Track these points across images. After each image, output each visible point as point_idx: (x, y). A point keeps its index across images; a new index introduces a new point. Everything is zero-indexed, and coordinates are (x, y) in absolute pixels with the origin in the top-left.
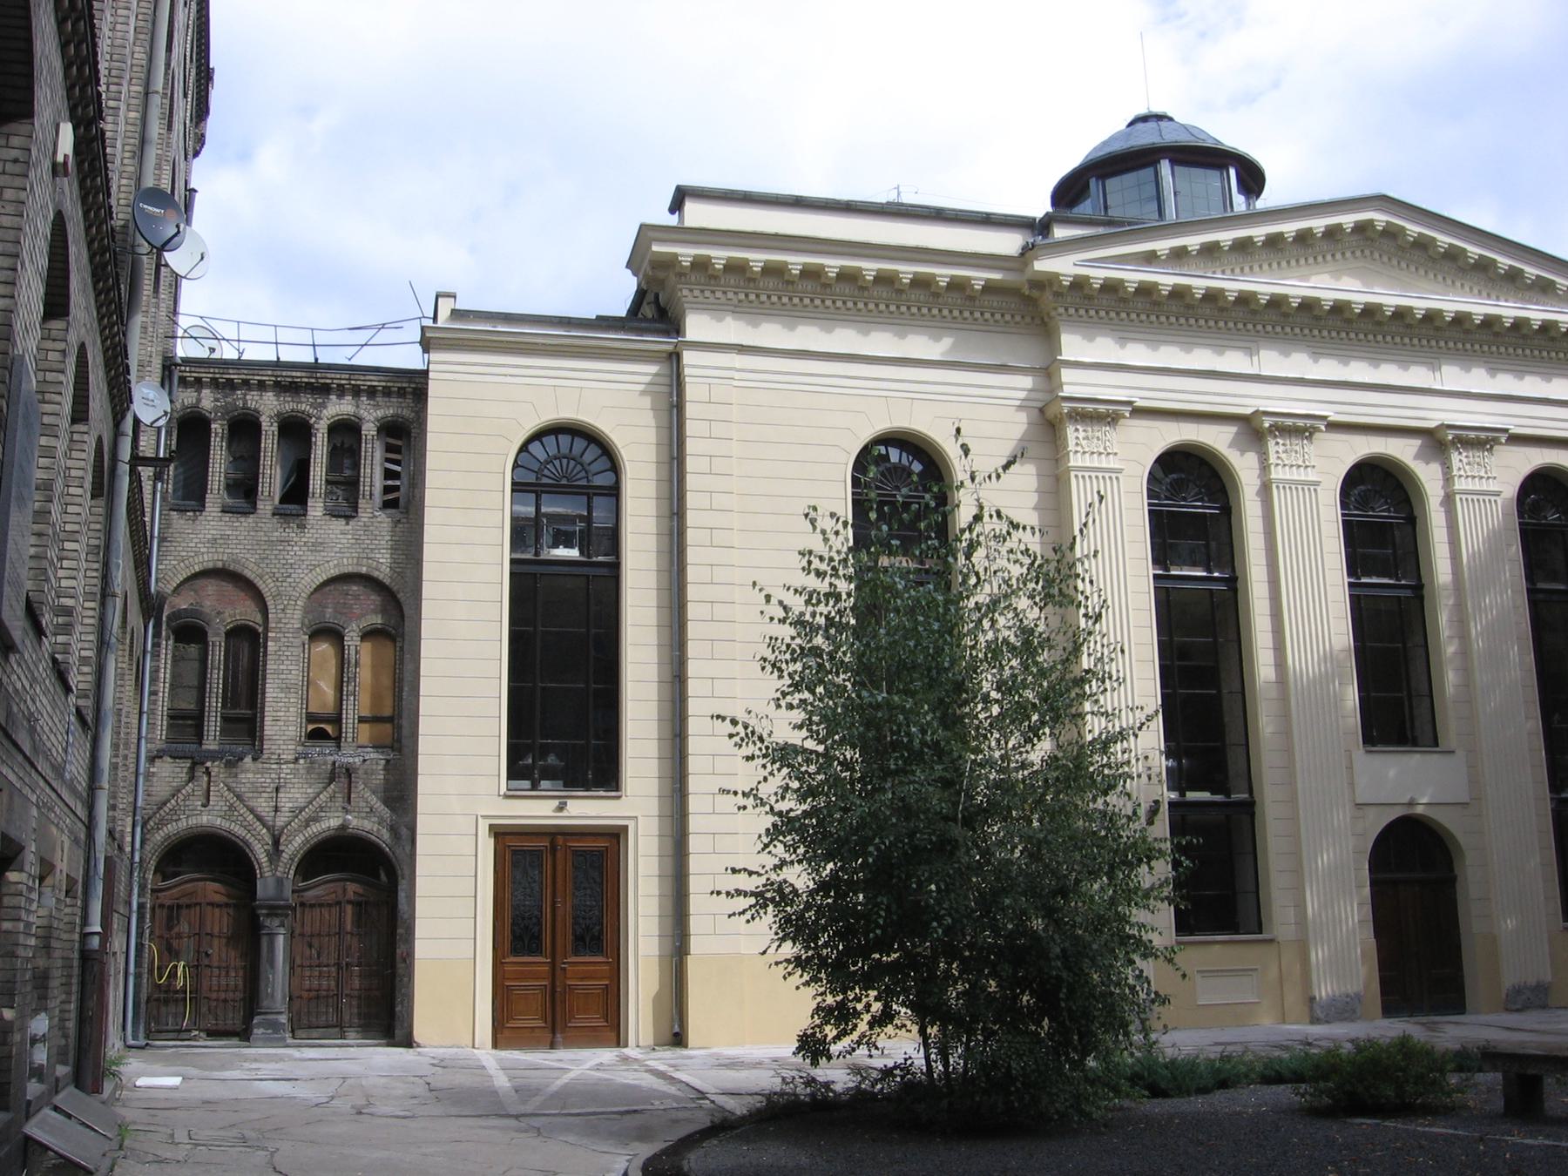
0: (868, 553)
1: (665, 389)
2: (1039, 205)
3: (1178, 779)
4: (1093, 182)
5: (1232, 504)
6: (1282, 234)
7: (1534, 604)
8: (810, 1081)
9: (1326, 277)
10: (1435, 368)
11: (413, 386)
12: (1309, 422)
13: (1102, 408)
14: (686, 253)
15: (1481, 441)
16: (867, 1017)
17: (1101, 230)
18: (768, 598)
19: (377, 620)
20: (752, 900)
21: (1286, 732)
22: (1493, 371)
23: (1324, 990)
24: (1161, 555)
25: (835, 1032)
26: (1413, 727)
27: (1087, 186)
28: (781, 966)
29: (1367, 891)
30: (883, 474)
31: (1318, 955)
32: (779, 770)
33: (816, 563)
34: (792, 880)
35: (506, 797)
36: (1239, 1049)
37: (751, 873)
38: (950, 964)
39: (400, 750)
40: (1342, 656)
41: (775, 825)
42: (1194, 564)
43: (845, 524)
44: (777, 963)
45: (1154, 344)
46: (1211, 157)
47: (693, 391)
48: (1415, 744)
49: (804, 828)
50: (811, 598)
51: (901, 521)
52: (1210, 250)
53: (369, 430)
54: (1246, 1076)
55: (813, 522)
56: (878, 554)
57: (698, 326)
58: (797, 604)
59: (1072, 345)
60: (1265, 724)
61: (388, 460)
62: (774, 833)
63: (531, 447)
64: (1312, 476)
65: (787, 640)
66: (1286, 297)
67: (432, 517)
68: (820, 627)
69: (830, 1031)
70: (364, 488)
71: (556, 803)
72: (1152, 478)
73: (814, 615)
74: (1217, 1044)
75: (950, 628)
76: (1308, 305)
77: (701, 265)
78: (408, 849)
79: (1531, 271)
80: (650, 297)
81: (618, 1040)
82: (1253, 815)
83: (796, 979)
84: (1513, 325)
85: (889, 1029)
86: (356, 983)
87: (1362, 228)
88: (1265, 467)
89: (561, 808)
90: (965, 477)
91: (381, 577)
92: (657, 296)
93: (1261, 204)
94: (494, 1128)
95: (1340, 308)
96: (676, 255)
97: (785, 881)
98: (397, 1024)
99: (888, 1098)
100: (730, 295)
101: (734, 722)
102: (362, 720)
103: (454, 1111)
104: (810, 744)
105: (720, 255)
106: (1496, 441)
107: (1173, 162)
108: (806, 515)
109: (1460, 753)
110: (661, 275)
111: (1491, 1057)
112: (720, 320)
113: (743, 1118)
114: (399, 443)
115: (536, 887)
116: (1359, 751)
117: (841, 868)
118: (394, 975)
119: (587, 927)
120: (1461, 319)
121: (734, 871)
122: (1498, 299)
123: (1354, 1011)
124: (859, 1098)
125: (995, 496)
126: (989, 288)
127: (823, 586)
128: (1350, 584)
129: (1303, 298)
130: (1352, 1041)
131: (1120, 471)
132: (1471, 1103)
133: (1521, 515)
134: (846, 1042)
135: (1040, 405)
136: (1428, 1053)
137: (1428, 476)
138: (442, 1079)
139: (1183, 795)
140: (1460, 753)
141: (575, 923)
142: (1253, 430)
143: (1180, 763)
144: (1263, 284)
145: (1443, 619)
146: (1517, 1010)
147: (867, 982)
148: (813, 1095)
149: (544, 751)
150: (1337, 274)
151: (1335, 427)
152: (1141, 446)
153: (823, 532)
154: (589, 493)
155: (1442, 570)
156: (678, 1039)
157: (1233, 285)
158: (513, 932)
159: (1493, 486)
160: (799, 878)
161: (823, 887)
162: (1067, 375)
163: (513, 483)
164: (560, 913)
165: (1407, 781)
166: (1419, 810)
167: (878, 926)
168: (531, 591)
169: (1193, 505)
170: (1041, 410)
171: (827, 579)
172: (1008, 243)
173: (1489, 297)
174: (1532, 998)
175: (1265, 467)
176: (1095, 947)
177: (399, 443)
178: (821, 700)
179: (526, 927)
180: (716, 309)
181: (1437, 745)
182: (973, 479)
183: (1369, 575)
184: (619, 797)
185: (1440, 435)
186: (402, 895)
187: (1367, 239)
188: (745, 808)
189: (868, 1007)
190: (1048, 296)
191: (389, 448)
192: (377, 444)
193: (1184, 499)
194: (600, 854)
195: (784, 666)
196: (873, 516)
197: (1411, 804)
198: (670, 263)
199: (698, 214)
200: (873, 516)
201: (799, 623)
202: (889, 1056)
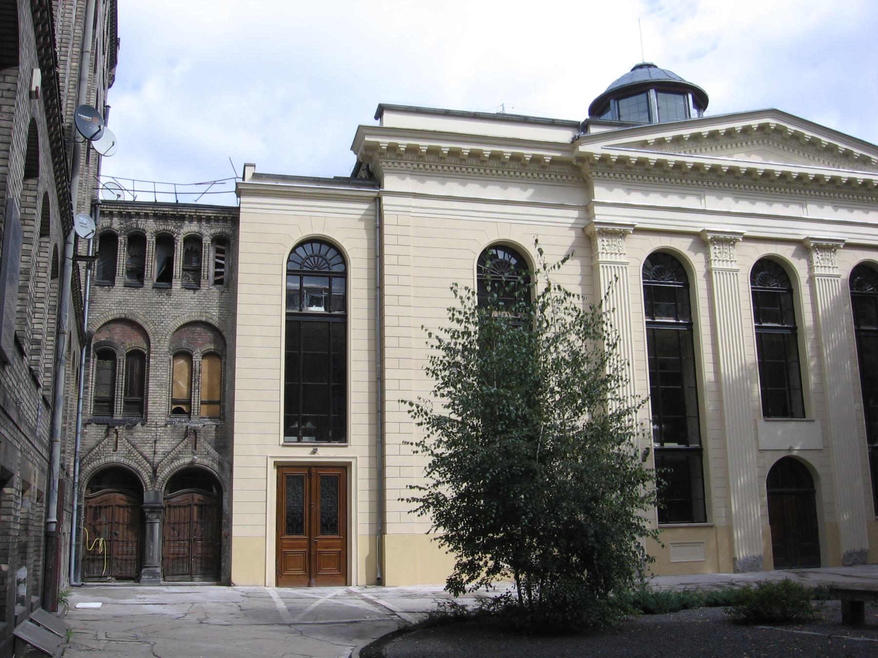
0: (486, 309)
1: (373, 218)
2: (582, 115)
3: (660, 436)
4: (612, 102)
5: (690, 282)
6: (718, 131)
7: (859, 338)
8: (454, 605)
9: (743, 155)
10: (803, 206)
11: (231, 216)
12: (733, 236)
13: (617, 228)
14: (384, 142)
15: (829, 247)
16: (485, 569)
17: (617, 129)
18: (430, 335)
19: (211, 347)
20: (421, 504)
21: (720, 409)
22: (836, 208)
23: (742, 554)
24: (650, 311)
25: (467, 578)
26: (791, 407)
27: (609, 104)
28: (437, 541)
29: (765, 498)
30: (494, 265)
31: (738, 534)
32: (436, 431)
33: (457, 315)
34: (443, 492)
35: (284, 446)
36: (694, 587)
37: (420, 489)
38: (532, 539)
39: (224, 420)
40: (752, 367)
41: (434, 462)
42: (669, 316)
43: (473, 293)
44: (435, 539)
45: (646, 192)
46: (678, 88)
47: (388, 219)
48: (792, 416)
49: (450, 463)
50: (454, 334)
51: (505, 292)
52: (678, 140)
53: (207, 240)
54: (698, 602)
55: (455, 292)
56: (491, 310)
57: (391, 182)
58: (447, 338)
59: (600, 193)
60: (708, 405)
61: (217, 257)
62: (434, 466)
63: (297, 250)
64: (734, 266)
65: (441, 358)
66: (720, 166)
67: (242, 289)
68: (459, 351)
69: (465, 577)
70: (204, 273)
71: (311, 449)
72: (645, 267)
73: (456, 344)
74: (681, 584)
75: (532, 352)
76: (733, 171)
77: (393, 148)
78: (228, 475)
79: (857, 152)
80: (364, 166)
81: (346, 582)
82: (701, 456)
83: (446, 548)
84: (847, 182)
85: (498, 576)
86: (200, 550)
87: (762, 128)
88: (708, 261)
89: (314, 452)
90: (540, 267)
91: (213, 323)
92: (368, 166)
93: (706, 114)
94: (276, 631)
95: (750, 172)
96: (378, 143)
97: (440, 493)
98: (223, 573)
99: (497, 614)
100: (409, 165)
101: (411, 404)
102: (203, 403)
103: (254, 622)
104: (454, 416)
105: (403, 143)
106: (838, 247)
107: (657, 91)
108: (452, 288)
109: (818, 421)
110: (370, 154)
111: (835, 591)
112: (403, 179)
113: (416, 625)
114: (224, 248)
115: (300, 496)
116: (761, 420)
117: (471, 486)
118: (220, 546)
119: (329, 519)
120: (818, 179)
121: (411, 487)
122: (839, 167)
123: (758, 566)
124: (481, 615)
125: (557, 278)
126: (554, 161)
127: (461, 328)
128: (756, 327)
129: (730, 167)
130: (757, 583)
131: (627, 263)
132: (824, 617)
133: (851, 288)
134: (473, 583)
135: (582, 226)
136: (799, 589)
137: (800, 266)
138: (247, 604)
139: (662, 445)
140: (818, 421)
141: (322, 517)
142: (702, 241)
143: (661, 427)
144: (707, 159)
145: (808, 346)
146: (850, 565)
147: (486, 549)
148: (455, 613)
149: (305, 420)
150: (748, 154)
151: (747, 239)
152: (639, 250)
153: (461, 298)
154: (330, 276)
155: (807, 319)
156: (380, 581)
157: (690, 160)
158: (287, 521)
159: (836, 272)
160: (448, 491)
161: (461, 496)
162: (597, 210)
163: (288, 271)
164: (313, 511)
165: (788, 437)
166: (795, 453)
167: (492, 518)
168: (298, 331)
169: (668, 282)
170: (583, 230)
171: (463, 324)
172: (564, 136)
173: (834, 166)
174: (858, 558)
175: (708, 261)
176: (613, 530)
177: (224, 248)
178: (460, 392)
179: (295, 519)
180: (401, 173)
181: (805, 417)
182: (545, 268)
183: (766, 322)
184: (346, 446)
185: (806, 243)
186: (225, 501)
187: (766, 134)
188: (417, 452)
189: (486, 563)
190: (587, 166)
191: (218, 251)
192: (211, 249)
193: (663, 279)
194: (336, 478)
195: (439, 373)
196: (489, 289)
197: (790, 450)
198: (375, 147)
199: (391, 120)
200: (489, 289)
201: (448, 348)
202: (498, 591)
